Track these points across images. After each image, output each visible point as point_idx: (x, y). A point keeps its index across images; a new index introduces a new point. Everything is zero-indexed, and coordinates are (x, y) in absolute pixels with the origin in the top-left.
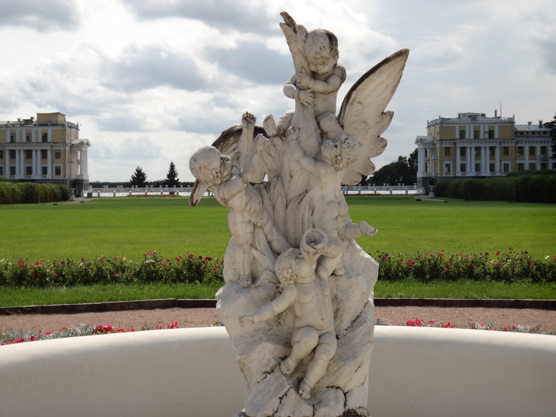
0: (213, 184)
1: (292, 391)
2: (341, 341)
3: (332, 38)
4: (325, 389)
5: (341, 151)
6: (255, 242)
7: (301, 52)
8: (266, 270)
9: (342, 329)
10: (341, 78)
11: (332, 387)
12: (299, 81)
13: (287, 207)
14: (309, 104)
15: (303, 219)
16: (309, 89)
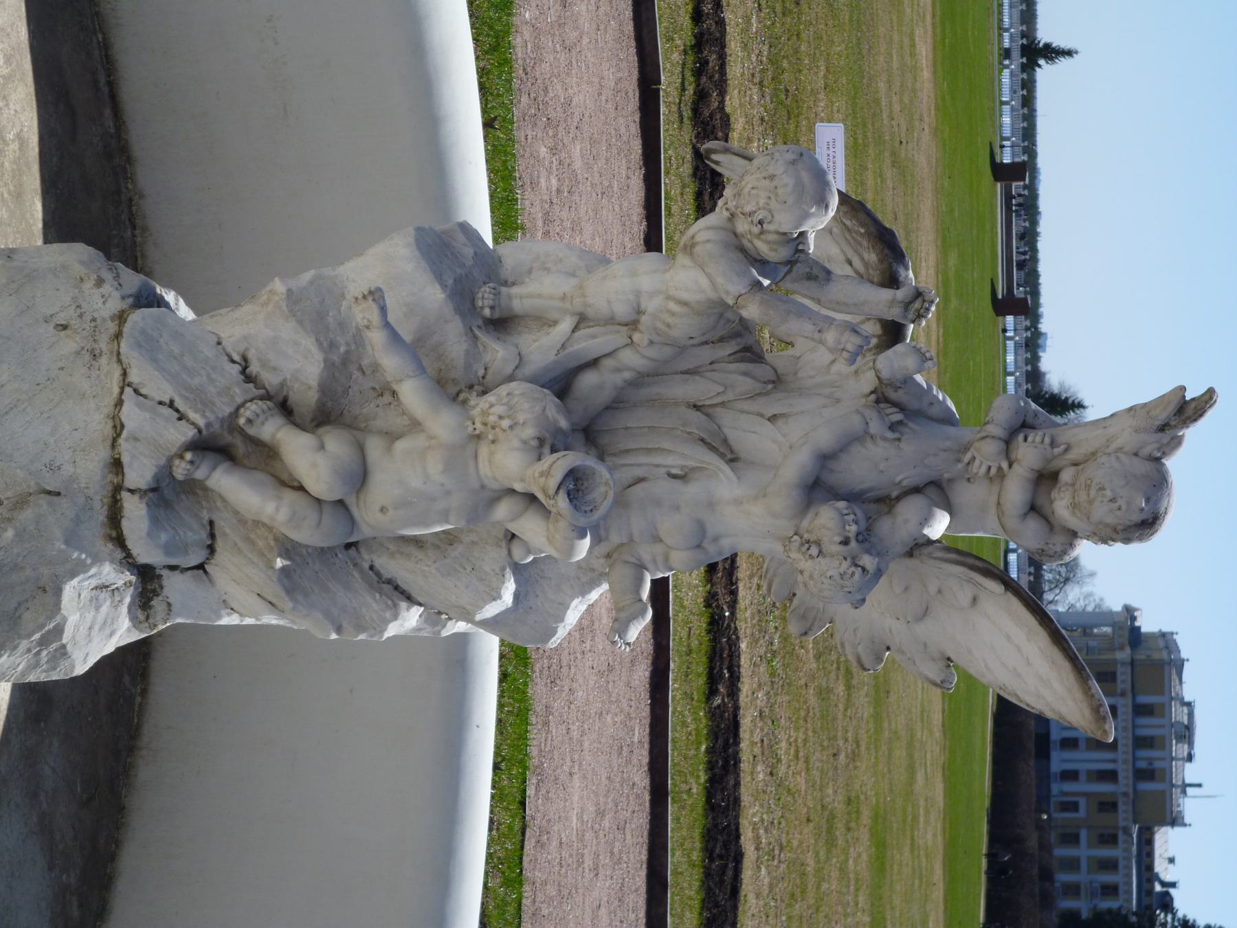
0: (734, 213)
1: (190, 433)
2: (340, 555)
3: (1146, 525)
4: (207, 518)
6: (592, 327)
7: (1109, 441)
8: (518, 358)
9: (374, 557)
10: (1043, 551)
11: (212, 536)
12: (1030, 439)
13: (696, 407)
14: (969, 463)
15: (660, 450)
16: (1010, 466)
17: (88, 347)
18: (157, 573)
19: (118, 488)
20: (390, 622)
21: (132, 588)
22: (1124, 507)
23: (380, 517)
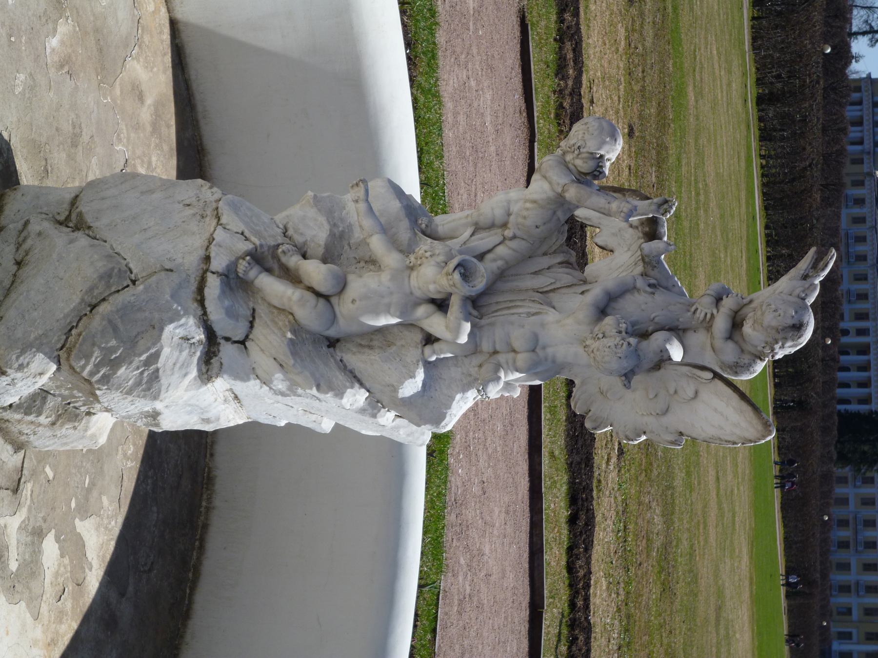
2: (324, 348)
4: (252, 306)
5: (611, 337)
9: (344, 355)
11: (254, 318)
17: (201, 213)
18: (218, 341)
19: (205, 271)
20: (348, 388)
21: (202, 346)
22: (782, 314)
23: (351, 306)
